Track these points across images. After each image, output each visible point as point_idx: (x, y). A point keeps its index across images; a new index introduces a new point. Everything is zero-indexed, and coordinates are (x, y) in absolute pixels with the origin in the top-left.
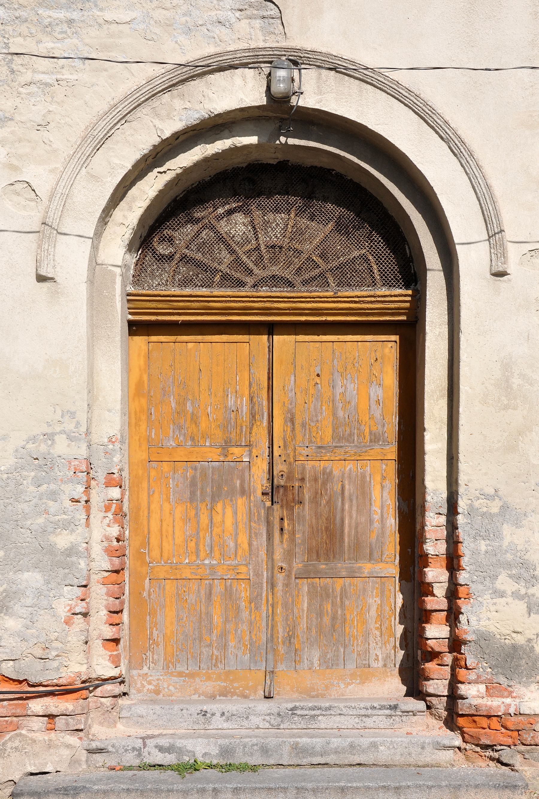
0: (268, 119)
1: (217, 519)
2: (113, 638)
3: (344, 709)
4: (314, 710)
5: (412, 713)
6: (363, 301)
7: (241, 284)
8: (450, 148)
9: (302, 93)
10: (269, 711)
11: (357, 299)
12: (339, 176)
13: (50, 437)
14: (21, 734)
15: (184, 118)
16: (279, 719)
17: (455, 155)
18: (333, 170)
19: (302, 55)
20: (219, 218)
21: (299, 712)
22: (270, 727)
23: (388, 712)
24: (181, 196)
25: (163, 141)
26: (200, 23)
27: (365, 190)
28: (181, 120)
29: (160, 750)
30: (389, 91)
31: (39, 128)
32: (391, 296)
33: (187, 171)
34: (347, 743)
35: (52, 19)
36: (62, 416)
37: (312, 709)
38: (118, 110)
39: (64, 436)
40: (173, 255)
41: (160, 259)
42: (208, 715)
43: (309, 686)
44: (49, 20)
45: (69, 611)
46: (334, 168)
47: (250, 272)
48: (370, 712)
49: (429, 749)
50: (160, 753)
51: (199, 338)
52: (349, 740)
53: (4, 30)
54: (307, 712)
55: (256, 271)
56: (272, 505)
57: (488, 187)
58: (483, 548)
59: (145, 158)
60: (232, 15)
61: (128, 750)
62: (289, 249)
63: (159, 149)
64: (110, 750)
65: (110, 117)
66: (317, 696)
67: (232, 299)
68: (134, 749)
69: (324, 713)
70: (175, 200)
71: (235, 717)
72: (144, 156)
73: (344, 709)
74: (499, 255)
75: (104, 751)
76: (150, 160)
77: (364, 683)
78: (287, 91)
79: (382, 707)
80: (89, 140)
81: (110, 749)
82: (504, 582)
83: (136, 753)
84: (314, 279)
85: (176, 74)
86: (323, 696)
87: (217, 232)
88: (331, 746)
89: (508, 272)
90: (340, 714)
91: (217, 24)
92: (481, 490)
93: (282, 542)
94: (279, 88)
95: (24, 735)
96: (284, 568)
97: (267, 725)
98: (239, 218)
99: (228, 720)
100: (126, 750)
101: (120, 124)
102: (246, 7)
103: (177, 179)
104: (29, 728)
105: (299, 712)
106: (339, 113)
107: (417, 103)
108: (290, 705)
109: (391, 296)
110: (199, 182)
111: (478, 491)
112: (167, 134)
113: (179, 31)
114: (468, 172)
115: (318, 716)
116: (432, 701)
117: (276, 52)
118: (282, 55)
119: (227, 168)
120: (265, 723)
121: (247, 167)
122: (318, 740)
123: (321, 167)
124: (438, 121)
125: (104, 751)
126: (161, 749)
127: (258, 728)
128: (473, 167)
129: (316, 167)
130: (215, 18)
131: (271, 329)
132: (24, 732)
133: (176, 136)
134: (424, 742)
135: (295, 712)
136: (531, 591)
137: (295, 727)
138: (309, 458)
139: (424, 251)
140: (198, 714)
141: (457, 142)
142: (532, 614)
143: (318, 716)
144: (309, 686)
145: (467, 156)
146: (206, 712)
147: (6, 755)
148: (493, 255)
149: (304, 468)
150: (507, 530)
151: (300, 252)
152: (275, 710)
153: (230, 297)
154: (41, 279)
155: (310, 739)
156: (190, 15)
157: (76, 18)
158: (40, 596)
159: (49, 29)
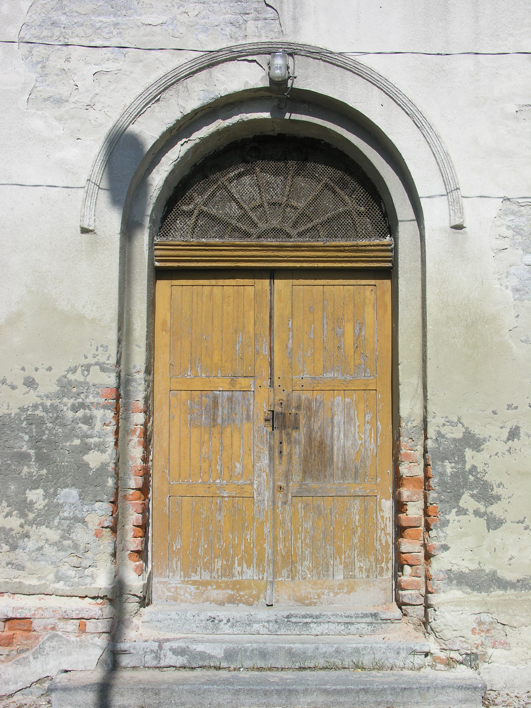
0: (270, 98)
1: (227, 441)
2: (136, 549)
3: (331, 617)
4: (306, 618)
5: (390, 621)
6: (347, 250)
7: (247, 235)
8: (414, 122)
9: (295, 78)
10: (268, 619)
11: (342, 248)
12: (327, 145)
13: (87, 368)
14: (57, 635)
15: (201, 98)
16: (276, 626)
17: (419, 128)
18: (322, 140)
19: (295, 48)
20: (230, 181)
21: (293, 620)
22: (269, 633)
23: (369, 620)
24: (200, 162)
25: (185, 117)
26: (216, 24)
27: (348, 156)
28: (199, 99)
29: (174, 653)
30: (364, 76)
31: (87, 107)
32: (371, 246)
33: (203, 140)
34: (334, 649)
35: (102, 23)
36: (97, 350)
37: (304, 617)
38: (149, 92)
39: (98, 367)
40: (193, 211)
41: (182, 214)
42: (216, 621)
43: (303, 594)
44: (100, 24)
45: (99, 524)
46: (323, 139)
47: (256, 225)
48: (353, 620)
49: (403, 654)
50: (174, 656)
51: (213, 282)
52: (335, 646)
53: (65, 32)
54: (299, 620)
55: (260, 225)
56: (273, 430)
57: (447, 154)
58: (449, 470)
59: (170, 130)
60: (240, 18)
61: (147, 652)
62: (287, 206)
63: (182, 123)
64: (132, 651)
65: (144, 98)
66: (310, 604)
67: (240, 248)
68: (152, 651)
69: (315, 620)
70: (195, 165)
71: (239, 623)
72: (170, 128)
73: (331, 617)
74: (456, 211)
75: (127, 652)
76: (174, 132)
77: (350, 592)
78: (283, 75)
79: (365, 616)
80: (126, 117)
81: (132, 651)
82: (467, 501)
83: (153, 655)
84: (308, 230)
85: (196, 63)
86: (315, 604)
87: (229, 192)
88: (320, 651)
89: (464, 226)
90: (329, 622)
91: (229, 25)
92: (447, 417)
93: (280, 464)
94: (278, 73)
95: (60, 636)
96: (282, 487)
97: (266, 631)
98: (246, 180)
99: (233, 626)
100: (146, 652)
101: (151, 103)
102: (252, 11)
103: (196, 147)
104: (64, 630)
105: (293, 620)
106: (325, 93)
107: (387, 85)
108: (286, 614)
109: (371, 246)
110: (215, 151)
111: (444, 419)
112: (188, 110)
113: (200, 30)
114: (429, 142)
115: (310, 623)
116: (407, 610)
117: (274, 46)
118: (279, 48)
119: (237, 139)
120: (265, 629)
121: (253, 138)
122: (308, 646)
123: (312, 138)
124: (404, 100)
125: (127, 652)
126: (175, 652)
127: (259, 634)
128: (433, 138)
129: (309, 138)
130: (228, 20)
131: (272, 274)
132: (60, 633)
133: (195, 112)
134: (399, 648)
135: (290, 620)
136: (490, 509)
137: (290, 633)
138: (304, 388)
139: (396, 207)
140: (208, 620)
141: (419, 117)
142: (490, 530)
143: (310, 623)
144: (303, 594)
145: (428, 129)
146: (214, 618)
147: (45, 653)
148: (451, 211)
149: (300, 398)
150: (468, 453)
151: (296, 208)
152: (273, 618)
153: (239, 247)
154: (85, 231)
155: (302, 645)
156: (208, 18)
157: (121, 22)
158: (75, 510)
159: (99, 31)
